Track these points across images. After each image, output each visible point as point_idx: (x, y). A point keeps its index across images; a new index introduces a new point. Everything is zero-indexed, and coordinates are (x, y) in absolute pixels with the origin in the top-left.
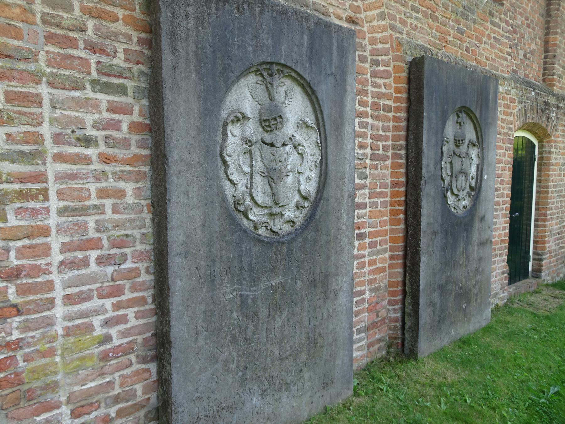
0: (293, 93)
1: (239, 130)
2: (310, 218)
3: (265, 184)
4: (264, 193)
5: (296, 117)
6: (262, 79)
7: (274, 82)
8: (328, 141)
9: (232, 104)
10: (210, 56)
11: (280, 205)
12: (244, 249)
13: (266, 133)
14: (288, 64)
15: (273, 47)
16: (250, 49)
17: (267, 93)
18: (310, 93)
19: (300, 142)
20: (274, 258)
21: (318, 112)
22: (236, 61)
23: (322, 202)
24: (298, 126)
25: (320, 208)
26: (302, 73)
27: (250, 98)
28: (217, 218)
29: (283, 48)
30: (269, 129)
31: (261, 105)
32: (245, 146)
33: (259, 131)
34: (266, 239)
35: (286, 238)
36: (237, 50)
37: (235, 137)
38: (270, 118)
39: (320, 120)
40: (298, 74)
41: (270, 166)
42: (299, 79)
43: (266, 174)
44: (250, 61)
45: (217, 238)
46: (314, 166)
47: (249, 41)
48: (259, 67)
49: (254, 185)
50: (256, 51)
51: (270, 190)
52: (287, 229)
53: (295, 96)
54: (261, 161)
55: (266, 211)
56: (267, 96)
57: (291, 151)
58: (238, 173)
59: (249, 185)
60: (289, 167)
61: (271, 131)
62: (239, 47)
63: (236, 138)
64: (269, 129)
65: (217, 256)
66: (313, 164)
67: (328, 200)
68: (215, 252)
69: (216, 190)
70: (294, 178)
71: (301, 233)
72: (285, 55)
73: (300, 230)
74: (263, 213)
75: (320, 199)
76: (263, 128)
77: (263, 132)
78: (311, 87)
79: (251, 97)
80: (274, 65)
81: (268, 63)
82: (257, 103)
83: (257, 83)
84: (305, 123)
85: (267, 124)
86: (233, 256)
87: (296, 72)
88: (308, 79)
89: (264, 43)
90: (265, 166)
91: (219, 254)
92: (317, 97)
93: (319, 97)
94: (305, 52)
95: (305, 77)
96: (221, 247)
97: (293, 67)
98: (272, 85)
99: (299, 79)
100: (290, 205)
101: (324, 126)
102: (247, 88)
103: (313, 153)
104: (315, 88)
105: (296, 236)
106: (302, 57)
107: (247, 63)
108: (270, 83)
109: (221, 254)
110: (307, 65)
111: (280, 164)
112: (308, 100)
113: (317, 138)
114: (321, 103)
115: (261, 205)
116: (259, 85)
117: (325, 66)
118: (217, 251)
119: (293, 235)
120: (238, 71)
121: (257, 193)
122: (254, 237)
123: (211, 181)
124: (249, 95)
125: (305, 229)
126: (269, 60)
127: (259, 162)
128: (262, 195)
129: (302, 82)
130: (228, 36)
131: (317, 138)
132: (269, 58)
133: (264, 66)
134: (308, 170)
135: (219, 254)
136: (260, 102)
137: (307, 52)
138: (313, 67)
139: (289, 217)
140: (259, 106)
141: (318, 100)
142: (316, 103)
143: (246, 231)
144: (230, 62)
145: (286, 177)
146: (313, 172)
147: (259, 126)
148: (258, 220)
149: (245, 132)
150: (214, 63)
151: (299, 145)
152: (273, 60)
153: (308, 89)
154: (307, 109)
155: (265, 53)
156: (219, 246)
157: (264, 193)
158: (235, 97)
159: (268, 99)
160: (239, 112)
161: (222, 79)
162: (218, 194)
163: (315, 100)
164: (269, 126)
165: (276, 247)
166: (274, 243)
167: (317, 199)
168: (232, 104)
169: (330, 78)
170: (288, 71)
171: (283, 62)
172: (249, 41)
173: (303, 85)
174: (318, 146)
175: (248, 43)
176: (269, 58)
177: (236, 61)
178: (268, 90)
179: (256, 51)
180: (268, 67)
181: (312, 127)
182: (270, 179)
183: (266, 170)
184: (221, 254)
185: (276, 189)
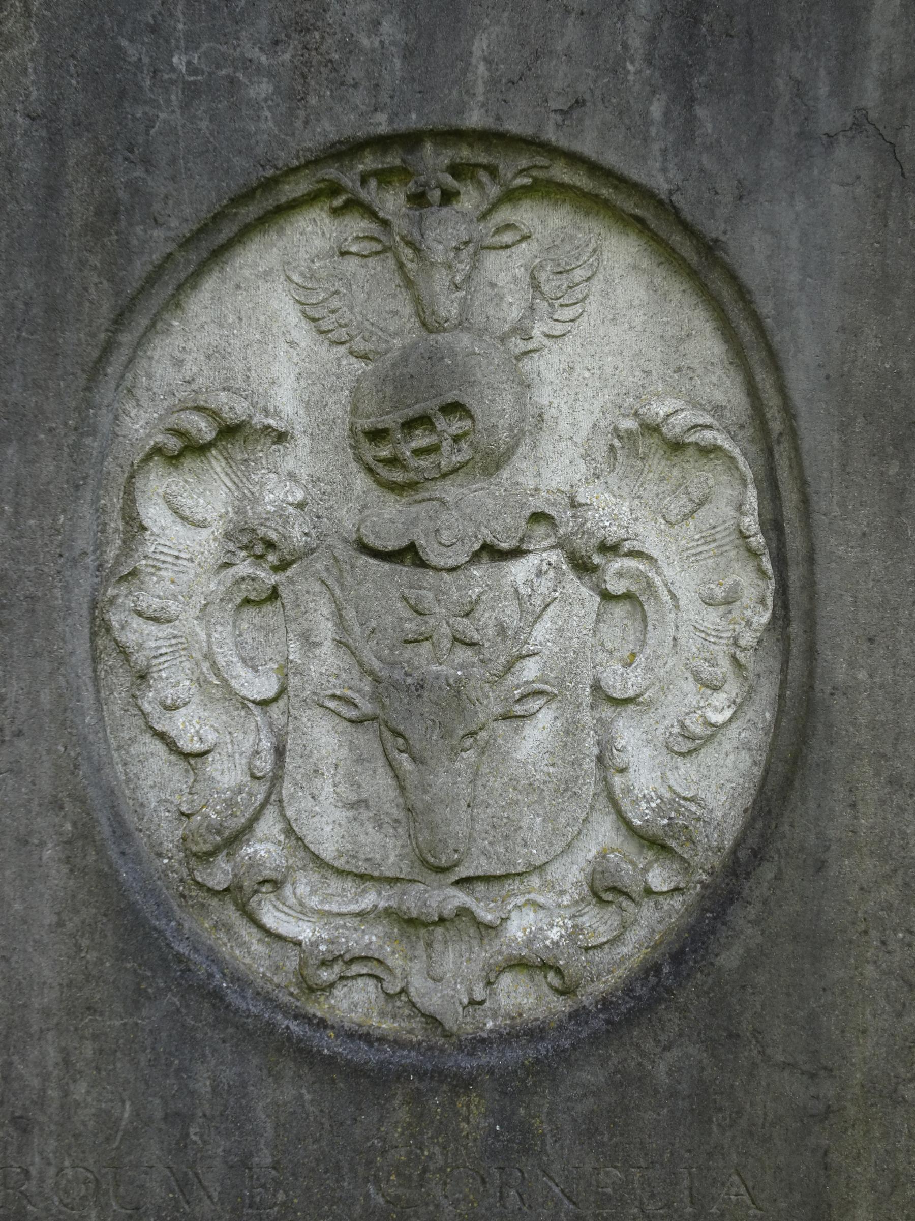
0: (579, 274)
1: (223, 494)
2: (677, 958)
3: (360, 760)
4: (352, 806)
5: (607, 396)
6: (373, 228)
7: (431, 235)
8: (819, 519)
9: (190, 368)
10: (30, 165)
11: (463, 872)
12: (203, 1086)
13: (391, 497)
14: (512, 126)
15: (408, 53)
16: (264, 88)
17: (404, 295)
18: (693, 258)
19: (614, 533)
20: (401, 1155)
21: (756, 357)
22: (173, 161)
23: (767, 872)
24: (612, 448)
25: (752, 912)
26: (611, 159)
27: (303, 334)
28: (50, 919)
29: (480, 45)
30: (398, 476)
31: (364, 357)
32: (244, 568)
33: (350, 487)
34: (365, 1055)
35: (485, 1059)
36: (185, 106)
37: (201, 525)
38: (390, 421)
39: (772, 401)
40: (594, 168)
41: (393, 665)
42: (605, 192)
43: (367, 707)
44: (260, 150)
45: (46, 1013)
46: (725, 665)
47: (255, 53)
48: (331, 172)
49: (291, 763)
50: (296, 98)
51: (393, 794)
52: (528, 1002)
53: (597, 285)
54: (339, 643)
55: (370, 899)
56: (408, 310)
57: (544, 585)
58: (208, 701)
59: (265, 764)
60: (530, 670)
61: (412, 486)
62: (192, 92)
63: (205, 533)
64: (398, 476)
65: (41, 1102)
66: (721, 652)
67: (821, 866)
68: (36, 1082)
69: (45, 785)
70: (571, 729)
71: (594, 1038)
72: (492, 83)
73: (598, 1023)
74: (355, 907)
75: (758, 855)
76: (370, 470)
77: (376, 491)
78: (688, 229)
79: (305, 325)
80: (428, 148)
81: (382, 143)
82: (343, 349)
83: (344, 254)
84: (651, 429)
85: (385, 452)
86: (136, 1114)
87: (574, 159)
88: (660, 184)
89: (350, 47)
90: (366, 671)
91: (53, 1093)
92: (732, 277)
93: (750, 277)
94: (636, 42)
95: (635, 174)
96: (66, 1062)
97: (551, 135)
98: (417, 250)
99: (605, 192)
100: (555, 871)
101: (793, 433)
102: (280, 285)
103: (719, 593)
104: (713, 229)
105: (559, 1052)
106: (616, 69)
107: (238, 162)
108: (410, 244)
109: (66, 1094)
110: (656, 110)
111: (463, 654)
112: (691, 299)
113: (739, 508)
114: (766, 307)
115: (340, 863)
116: (352, 264)
117: (800, 89)
118: (45, 1078)
119: (543, 1048)
120: (188, 211)
121: (307, 803)
122: (270, 1028)
123: (22, 744)
124: (291, 315)
125: (631, 1018)
126: (382, 124)
127: (327, 648)
128: (341, 815)
129: (630, 206)
130: (132, 52)
131: (739, 508)
132: (382, 117)
133: (369, 162)
134: (690, 686)
135: (53, 1093)
136: (360, 345)
137: (652, 39)
138: (701, 112)
139: (530, 941)
140: (359, 366)
141: (743, 293)
142: (735, 311)
143: (217, 995)
144: (139, 172)
145: (503, 727)
146: (719, 699)
147: (354, 466)
148: (315, 944)
149: (255, 500)
150: (53, 193)
151: (609, 549)
152: (413, 121)
153: (676, 238)
154: (689, 347)
155: (359, 98)
156: (53, 1055)
157: (352, 806)
158: (210, 337)
159: (415, 322)
160: (199, 409)
161: (95, 261)
162: (57, 805)
163: (727, 294)
164: (393, 462)
165: (416, 1098)
166: (401, 1075)
167: (743, 855)
168: (190, 368)
169: (841, 152)
170: (524, 163)
171: (475, 119)
172: (255, 53)
173: (640, 220)
174: (754, 554)
175: (247, 63)
176: (382, 117)
177: (173, 161)
178: (409, 283)
179: (296, 98)
180: (393, 159)
181: (708, 451)
182: (387, 734)
183: (367, 686)
184: (66, 1094)
185: (425, 788)
